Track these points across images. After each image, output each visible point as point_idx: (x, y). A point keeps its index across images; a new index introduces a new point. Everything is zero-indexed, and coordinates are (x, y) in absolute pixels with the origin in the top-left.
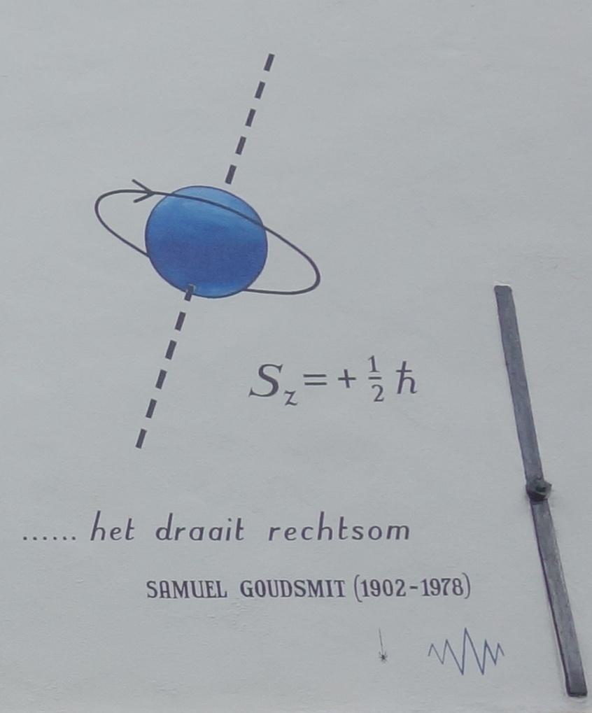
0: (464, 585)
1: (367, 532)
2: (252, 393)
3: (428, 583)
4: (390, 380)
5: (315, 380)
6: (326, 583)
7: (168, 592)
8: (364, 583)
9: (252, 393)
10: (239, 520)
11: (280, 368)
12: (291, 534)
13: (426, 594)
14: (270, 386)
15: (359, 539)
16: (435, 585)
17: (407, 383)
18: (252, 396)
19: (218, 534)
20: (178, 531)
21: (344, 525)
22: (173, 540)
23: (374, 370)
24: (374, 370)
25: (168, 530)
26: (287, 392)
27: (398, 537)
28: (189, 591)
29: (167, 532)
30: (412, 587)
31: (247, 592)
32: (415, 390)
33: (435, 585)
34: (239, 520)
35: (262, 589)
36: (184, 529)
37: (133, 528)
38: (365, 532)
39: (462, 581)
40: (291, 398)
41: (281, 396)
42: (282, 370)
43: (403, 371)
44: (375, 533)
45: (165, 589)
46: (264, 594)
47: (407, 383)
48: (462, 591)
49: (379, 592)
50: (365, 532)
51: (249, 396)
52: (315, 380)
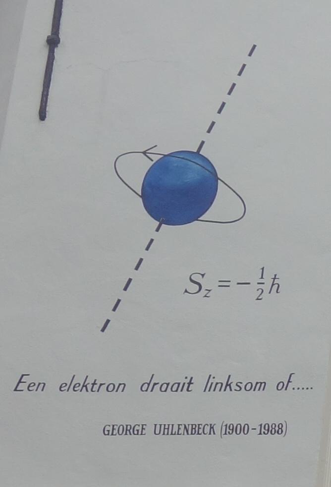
0: (284, 429)
1: (244, 387)
2: (186, 291)
3: (263, 426)
4: (268, 281)
5: (224, 284)
6: (159, 426)
7: (165, 429)
8: (226, 425)
9: (186, 291)
10: (192, 378)
11: (203, 275)
12: (64, 387)
13: (260, 434)
14: (197, 287)
15: (239, 391)
16: (267, 428)
17: (275, 287)
18: (186, 293)
19: (178, 387)
20: (155, 384)
21: (291, 381)
22: (96, 392)
23: (262, 278)
24: (262, 278)
25: (149, 384)
26: (207, 290)
27: (220, 390)
28: (157, 429)
29: (149, 386)
30: (255, 429)
31: (106, 433)
32: (278, 291)
33: (267, 428)
34: (192, 378)
35: (165, 430)
36: (104, 384)
37: (192, 383)
38: (243, 386)
39: (283, 425)
40: (208, 293)
41: (203, 292)
42: (204, 277)
43: (274, 279)
44: (248, 387)
45: (166, 430)
46: (240, 432)
47: (275, 287)
48: (282, 431)
49: (232, 432)
50: (243, 386)
51: (184, 293)
52: (224, 284)
